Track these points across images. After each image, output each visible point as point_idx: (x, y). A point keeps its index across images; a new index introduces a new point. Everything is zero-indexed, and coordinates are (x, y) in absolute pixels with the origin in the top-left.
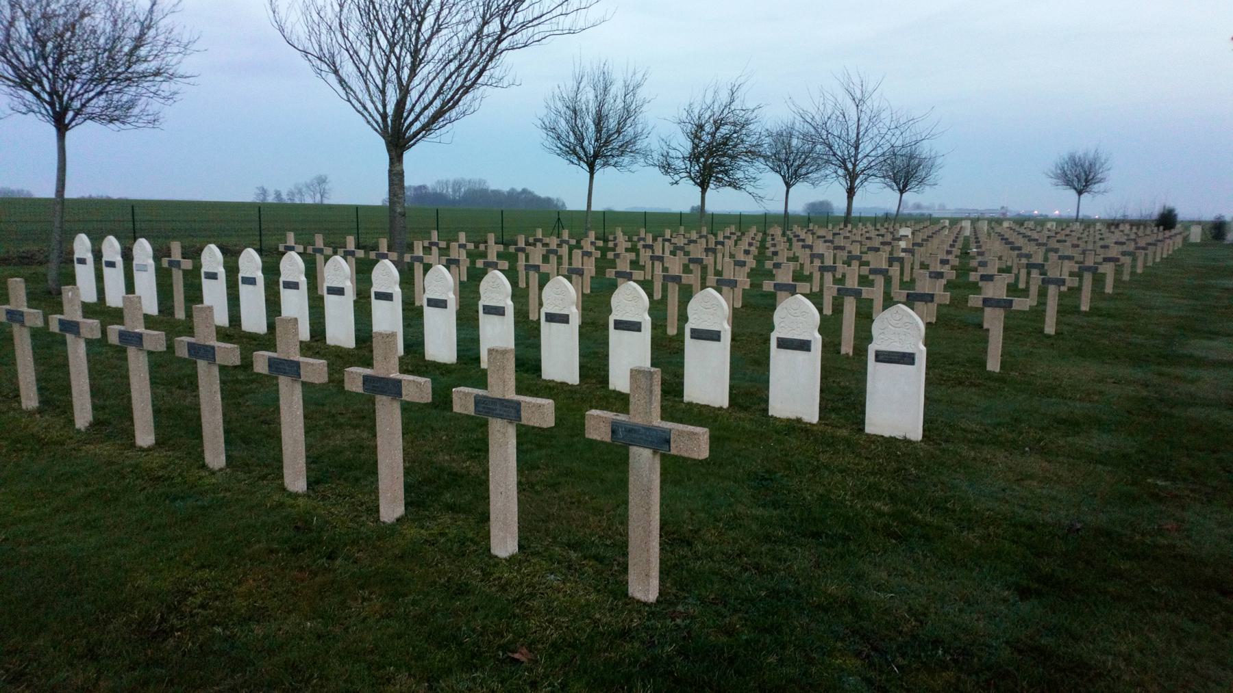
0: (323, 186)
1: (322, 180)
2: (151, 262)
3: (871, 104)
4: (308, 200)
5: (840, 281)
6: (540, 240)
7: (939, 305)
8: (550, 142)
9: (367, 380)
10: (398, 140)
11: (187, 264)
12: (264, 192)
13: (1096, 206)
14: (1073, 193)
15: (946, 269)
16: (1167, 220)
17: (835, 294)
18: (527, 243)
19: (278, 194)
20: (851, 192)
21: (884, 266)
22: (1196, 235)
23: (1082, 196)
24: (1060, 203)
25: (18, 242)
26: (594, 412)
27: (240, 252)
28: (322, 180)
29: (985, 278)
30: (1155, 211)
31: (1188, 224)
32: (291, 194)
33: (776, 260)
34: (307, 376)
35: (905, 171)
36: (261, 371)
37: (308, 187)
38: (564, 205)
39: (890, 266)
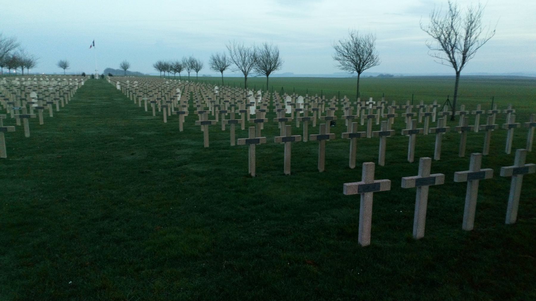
3: (25, 52)
13: (68, 71)
14: (63, 69)
16: (84, 75)
20: (23, 69)
22: (89, 77)
23: (224, 72)
24: (60, 71)
30: (81, 73)
31: (88, 75)
35: (28, 64)
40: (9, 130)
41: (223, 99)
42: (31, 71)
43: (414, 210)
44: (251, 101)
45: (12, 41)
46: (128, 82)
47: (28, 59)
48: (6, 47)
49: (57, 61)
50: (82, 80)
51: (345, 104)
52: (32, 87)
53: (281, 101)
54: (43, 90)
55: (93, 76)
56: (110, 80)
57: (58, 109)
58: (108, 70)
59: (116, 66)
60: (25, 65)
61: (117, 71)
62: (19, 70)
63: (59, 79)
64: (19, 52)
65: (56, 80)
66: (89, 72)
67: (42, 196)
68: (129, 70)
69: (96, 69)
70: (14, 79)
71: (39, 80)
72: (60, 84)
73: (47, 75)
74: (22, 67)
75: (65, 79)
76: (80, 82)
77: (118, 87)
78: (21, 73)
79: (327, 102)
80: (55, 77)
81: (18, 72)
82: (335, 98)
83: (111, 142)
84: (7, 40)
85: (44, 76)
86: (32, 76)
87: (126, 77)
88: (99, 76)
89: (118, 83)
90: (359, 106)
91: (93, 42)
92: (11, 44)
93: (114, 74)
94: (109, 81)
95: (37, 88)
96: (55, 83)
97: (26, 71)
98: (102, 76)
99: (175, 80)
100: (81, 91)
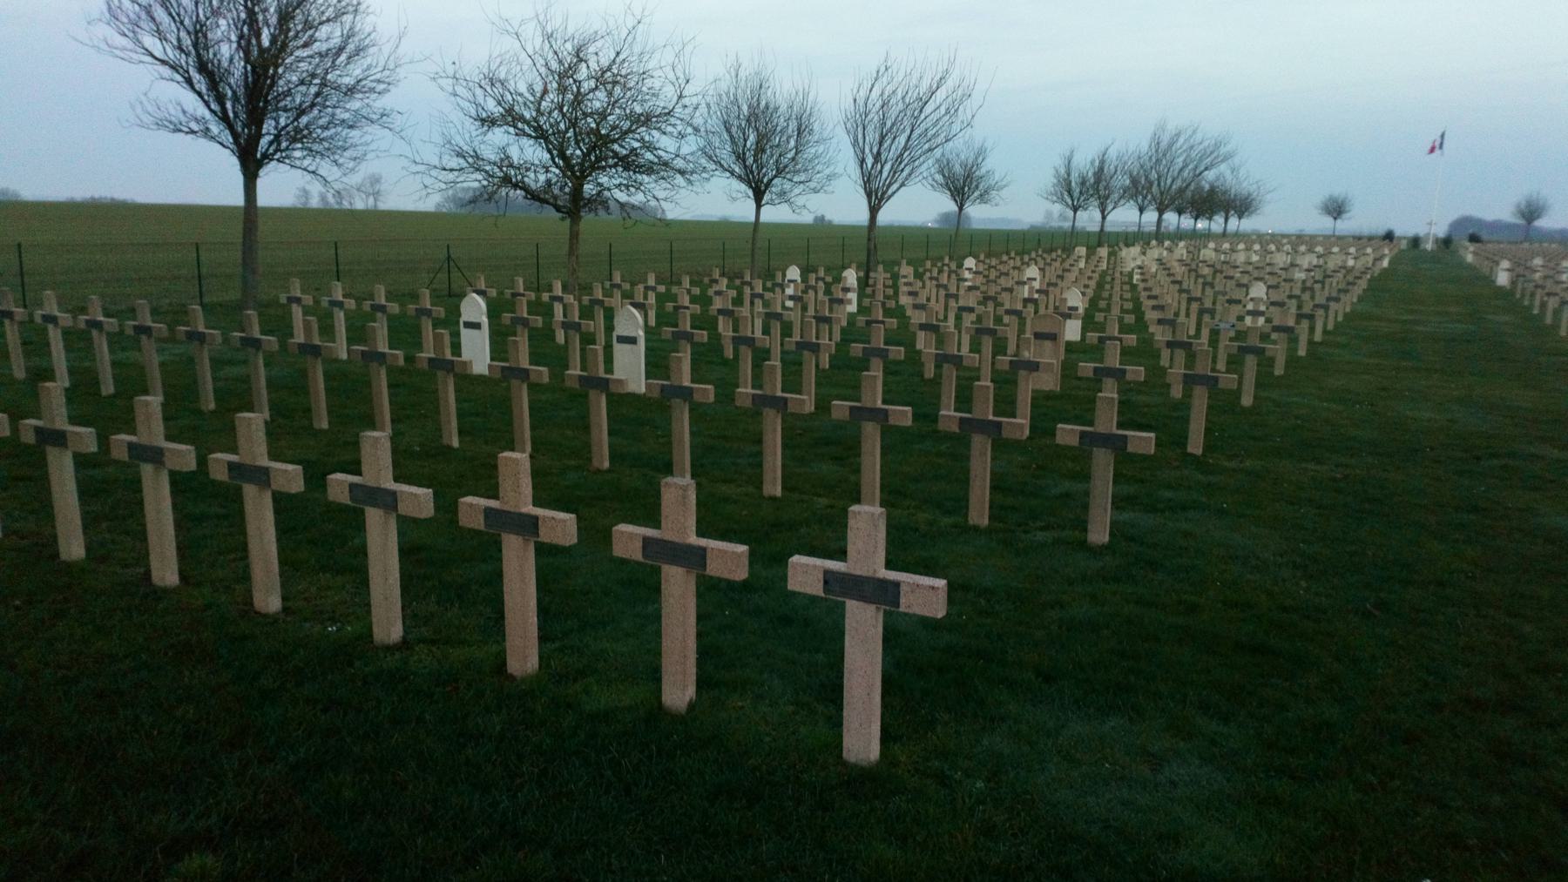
3: (1242, 172)
4: (359, 205)
8: (1059, 163)
9: (131, 447)
13: (1345, 226)
16: (1389, 236)
18: (765, 289)
21: (1291, 323)
22: (1404, 245)
24: (1322, 224)
26: (469, 499)
30: (1382, 231)
31: (1400, 238)
34: (278, 484)
35: (1242, 206)
36: (513, 537)
39: (1298, 322)
40: (891, 356)
41: (1225, 294)
42: (1247, 224)
43: (967, 481)
44: (1070, 303)
45: (1217, 145)
46: (1538, 261)
47: (1245, 192)
48: (1201, 160)
49: (1320, 195)
50: (1386, 251)
52: (1250, 268)
55: (1415, 242)
56: (1475, 253)
57: (1318, 337)
58: (1461, 223)
59: (1498, 209)
60: (1234, 208)
61: (1496, 226)
62: (1217, 224)
63: (1319, 249)
64: (1228, 174)
65: (1311, 251)
66: (1405, 227)
67: (1303, 584)
68: (1543, 223)
69: (1424, 215)
70: (1205, 247)
71: (1265, 252)
72: (1321, 261)
73: (1284, 236)
75: (1335, 250)
76: (1381, 258)
77: (1503, 279)
78: (1094, 227)
80: (1300, 241)
83: (1495, 456)
84: (1206, 144)
85: (1276, 239)
86: (1246, 238)
87: (1526, 245)
88: (1437, 240)
89: (1505, 264)
91: (1443, 136)
92: (1215, 154)
93: (1484, 236)
94: (1470, 258)
95: (1259, 272)
96: (1307, 260)
97: (1234, 224)
98: (1446, 242)
99: (1103, 252)
100: (1380, 286)
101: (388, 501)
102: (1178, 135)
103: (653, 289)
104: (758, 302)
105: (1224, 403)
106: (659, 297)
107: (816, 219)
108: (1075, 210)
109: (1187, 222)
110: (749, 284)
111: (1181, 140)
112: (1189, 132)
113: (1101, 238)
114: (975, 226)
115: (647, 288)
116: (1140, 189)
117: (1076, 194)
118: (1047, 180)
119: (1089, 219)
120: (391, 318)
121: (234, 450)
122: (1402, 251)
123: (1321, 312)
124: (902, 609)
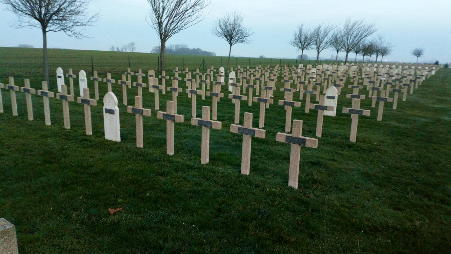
0: (133, 46)
1: (133, 44)
2: (86, 78)
3: (383, 40)
5: (248, 82)
6: (248, 70)
7: (273, 91)
8: (294, 34)
10: (164, 37)
11: (144, 85)
12: (113, 47)
14: (416, 57)
15: (277, 74)
16: (437, 63)
17: (247, 87)
19: (118, 49)
20: (377, 56)
24: (414, 59)
25: (35, 67)
27: (79, 72)
28: (133, 44)
29: (285, 76)
30: (434, 62)
31: (441, 65)
32: (122, 48)
33: (285, 74)
35: (384, 52)
37: (128, 46)
38: (215, 54)
42: (386, 59)
45: (370, 27)
51: (285, 72)
53: (289, 72)
54: (394, 78)
62: (373, 57)
69: (208, 50)
74: (377, 54)
79: (271, 70)
81: (371, 59)
82: (278, 66)
84: (365, 27)
90: (239, 71)
92: (369, 31)
100: (429, 83)
101: (140, 112)
102: (355, 24)
103: (213, 70)
104: (252, 76)
105: (388, 105)
106: (214, 72)
107: (260, 56)
108: (303, 50)
109: (360, 57)
110: (239, 69)
111: (356, 25)
112: (360, 22)
113: (316, 62)
114: (309, 59)
115: (211, 70)
116: (337, 43)
117: (303, 43)
118: (291, 37)
119: (311, 53)
120: (132, 76)
121: (24, 86)
122: (441, 68)
123: (330, 77)
124: (306, 146)
